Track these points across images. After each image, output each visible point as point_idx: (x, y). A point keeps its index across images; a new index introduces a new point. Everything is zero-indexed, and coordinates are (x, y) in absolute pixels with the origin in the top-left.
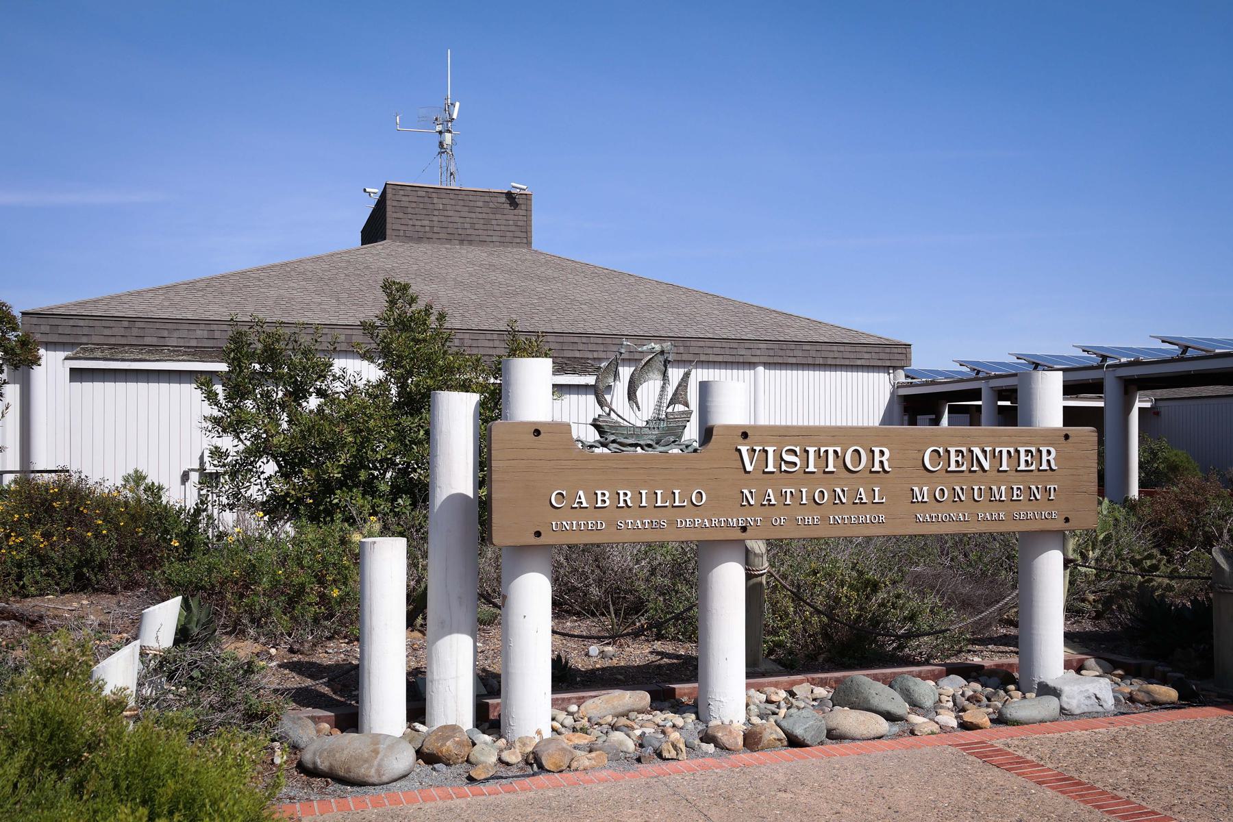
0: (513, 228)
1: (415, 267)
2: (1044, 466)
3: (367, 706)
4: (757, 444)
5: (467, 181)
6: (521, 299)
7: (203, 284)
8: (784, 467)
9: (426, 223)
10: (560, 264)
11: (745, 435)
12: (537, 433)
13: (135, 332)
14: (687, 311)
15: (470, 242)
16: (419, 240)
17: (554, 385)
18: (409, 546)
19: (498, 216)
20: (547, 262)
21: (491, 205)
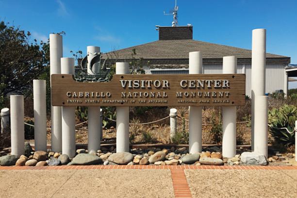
6: (184, 51)
12: (63, 77)
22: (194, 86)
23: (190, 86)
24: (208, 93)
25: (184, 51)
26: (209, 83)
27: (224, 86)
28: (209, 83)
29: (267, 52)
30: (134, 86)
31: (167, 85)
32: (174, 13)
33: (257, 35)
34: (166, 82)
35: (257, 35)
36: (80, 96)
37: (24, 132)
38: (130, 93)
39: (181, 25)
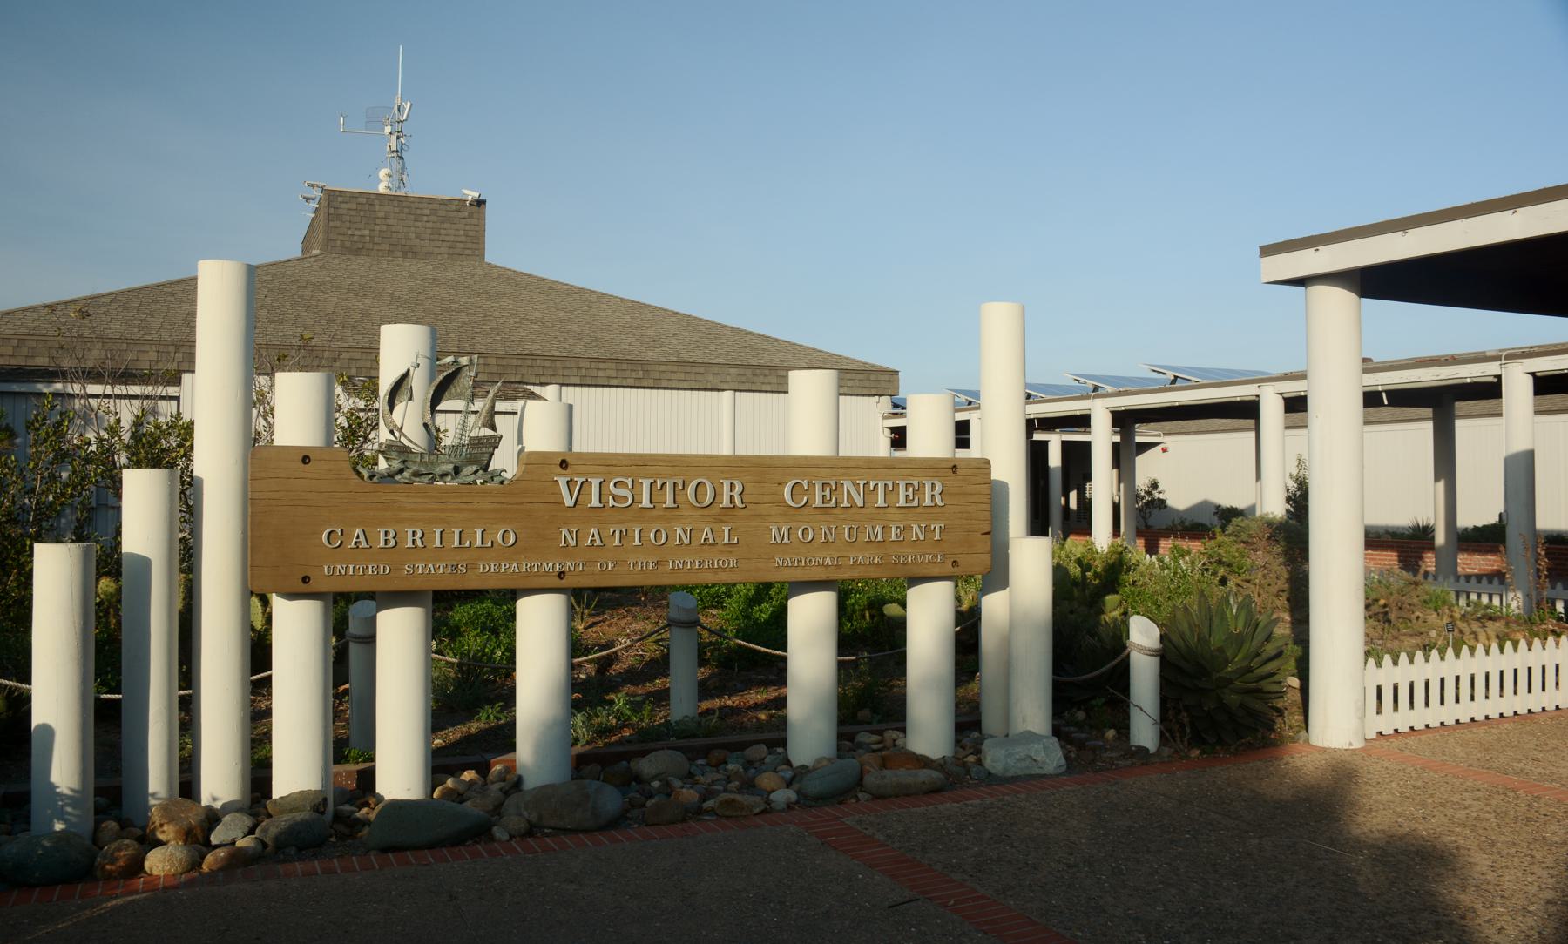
0: (463, 239)
1: (349, 281)
2: (928, 502)
3: (243, 698)
4: (578, 474)
5: (417, 188)
6: (463, 317)
7: (107, 300)
8: (611, 503)
9: (367, 232)
10: (516, 280)
11: (564, 464)
12: (306, 460)
13: (25, 351)
14: (651, 331)
15: (415, 254)
16: (358, 252)
17: (1500, 415)
18: (989, 474)
19: (447, 225)
20: (500, 276)
21: (441, 213)
22: (915, 503)
23: (818, 502)
24: (784, 530)
25: (463, 317)
26: (669, 487)
27: (928, 502)
28: (669, 487)
29: (1253, 434)
30: (611, 503)
31: (938, 498)
32: (388, 129)
33: (998, 322)
34: (732, 486)
35: (998, 322)
36: (382, 544)
37: (1480, 525)
38: (358, 531)
39: (426, 183)
